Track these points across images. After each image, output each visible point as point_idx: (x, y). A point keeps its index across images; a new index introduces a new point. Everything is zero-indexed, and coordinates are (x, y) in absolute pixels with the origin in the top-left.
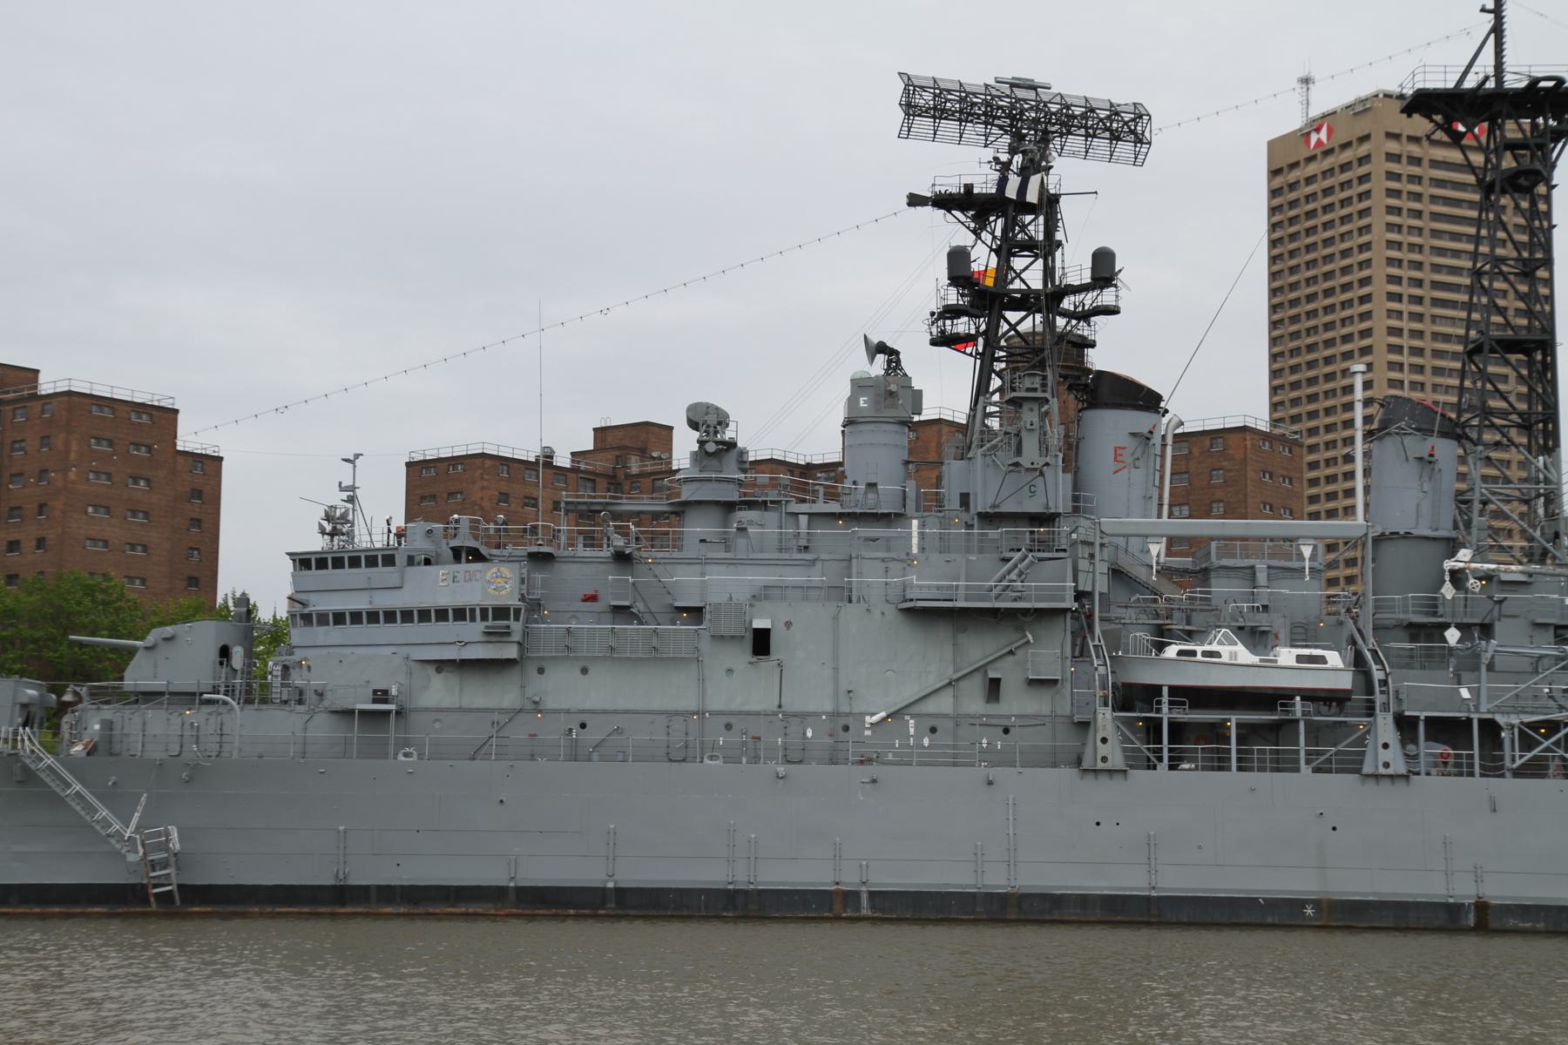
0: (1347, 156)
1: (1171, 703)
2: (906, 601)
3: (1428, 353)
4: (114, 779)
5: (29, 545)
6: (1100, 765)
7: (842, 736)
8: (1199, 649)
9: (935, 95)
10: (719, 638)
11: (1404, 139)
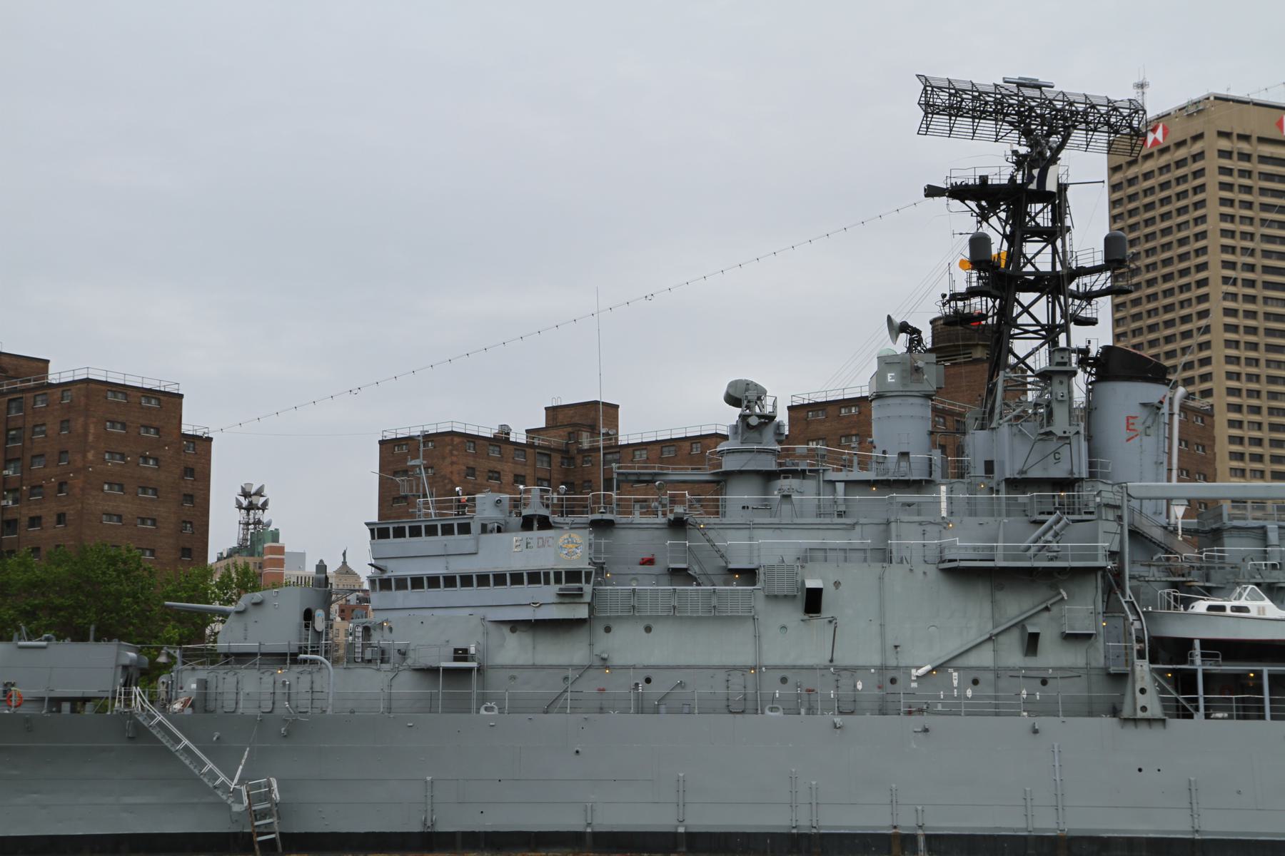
0: (1182, 153)
1: (1203, 655)
2: (944, 562)
3: (1261, 332)
4: (217, 734)
5: (49, 520)
6: (1140, 714)
7: (890, 688)
8: (1228, 604)
9: (950, 95)
10: (773, 598)
11: (1235, 137)
